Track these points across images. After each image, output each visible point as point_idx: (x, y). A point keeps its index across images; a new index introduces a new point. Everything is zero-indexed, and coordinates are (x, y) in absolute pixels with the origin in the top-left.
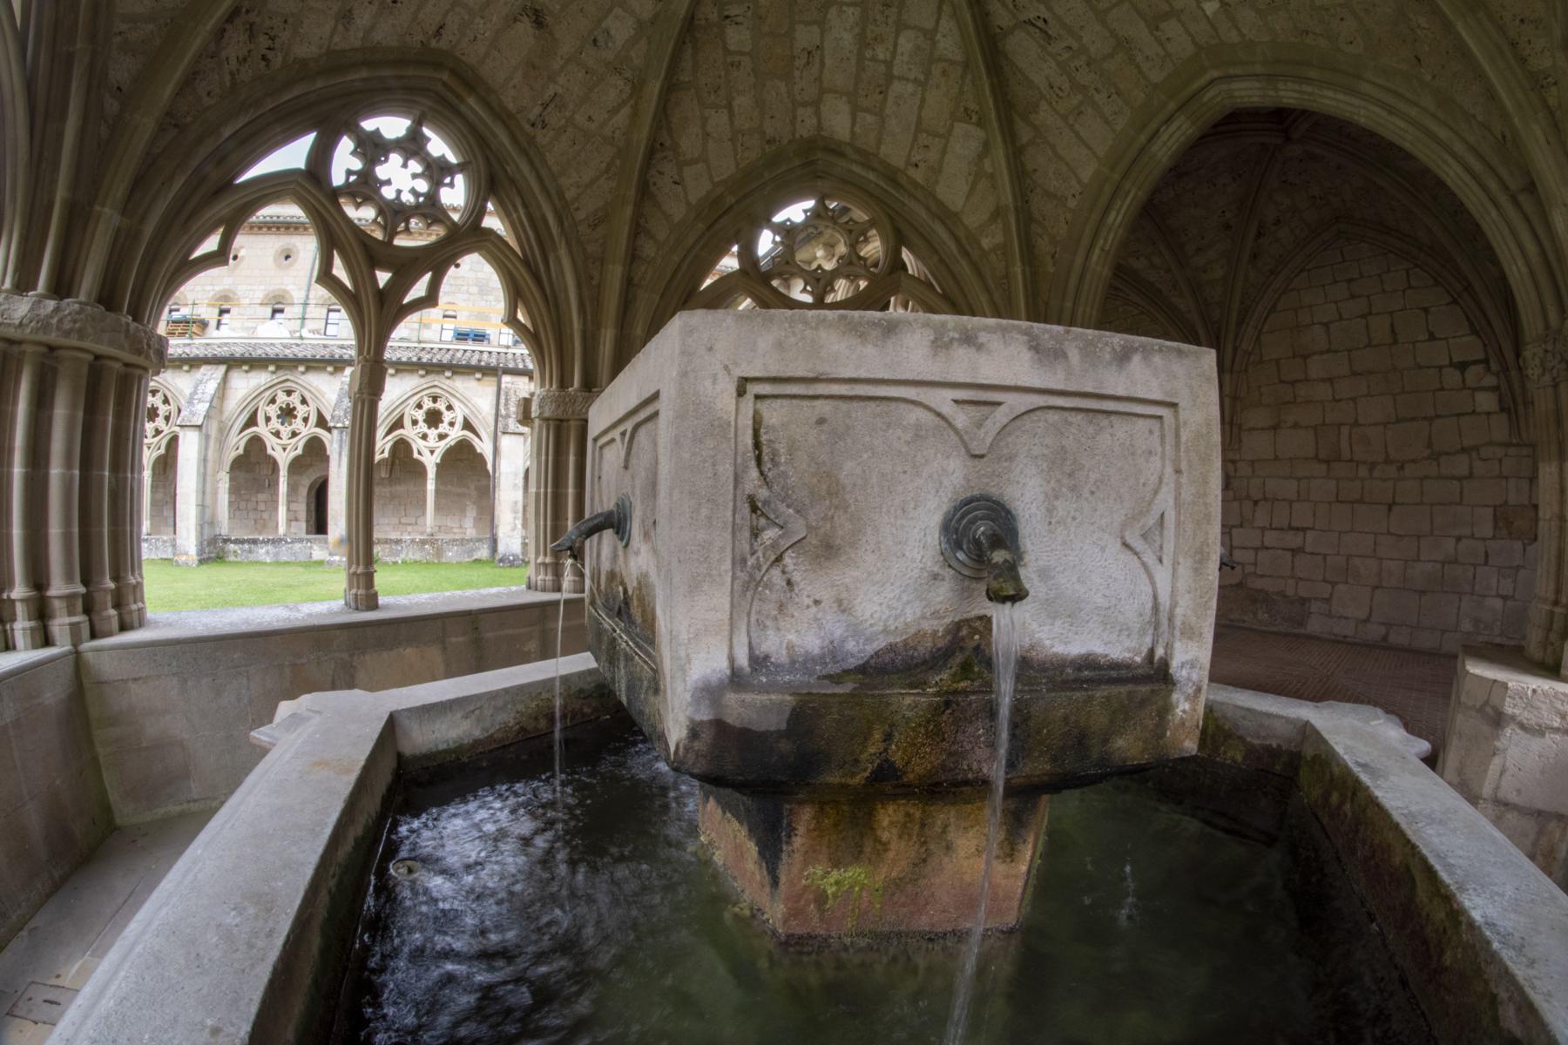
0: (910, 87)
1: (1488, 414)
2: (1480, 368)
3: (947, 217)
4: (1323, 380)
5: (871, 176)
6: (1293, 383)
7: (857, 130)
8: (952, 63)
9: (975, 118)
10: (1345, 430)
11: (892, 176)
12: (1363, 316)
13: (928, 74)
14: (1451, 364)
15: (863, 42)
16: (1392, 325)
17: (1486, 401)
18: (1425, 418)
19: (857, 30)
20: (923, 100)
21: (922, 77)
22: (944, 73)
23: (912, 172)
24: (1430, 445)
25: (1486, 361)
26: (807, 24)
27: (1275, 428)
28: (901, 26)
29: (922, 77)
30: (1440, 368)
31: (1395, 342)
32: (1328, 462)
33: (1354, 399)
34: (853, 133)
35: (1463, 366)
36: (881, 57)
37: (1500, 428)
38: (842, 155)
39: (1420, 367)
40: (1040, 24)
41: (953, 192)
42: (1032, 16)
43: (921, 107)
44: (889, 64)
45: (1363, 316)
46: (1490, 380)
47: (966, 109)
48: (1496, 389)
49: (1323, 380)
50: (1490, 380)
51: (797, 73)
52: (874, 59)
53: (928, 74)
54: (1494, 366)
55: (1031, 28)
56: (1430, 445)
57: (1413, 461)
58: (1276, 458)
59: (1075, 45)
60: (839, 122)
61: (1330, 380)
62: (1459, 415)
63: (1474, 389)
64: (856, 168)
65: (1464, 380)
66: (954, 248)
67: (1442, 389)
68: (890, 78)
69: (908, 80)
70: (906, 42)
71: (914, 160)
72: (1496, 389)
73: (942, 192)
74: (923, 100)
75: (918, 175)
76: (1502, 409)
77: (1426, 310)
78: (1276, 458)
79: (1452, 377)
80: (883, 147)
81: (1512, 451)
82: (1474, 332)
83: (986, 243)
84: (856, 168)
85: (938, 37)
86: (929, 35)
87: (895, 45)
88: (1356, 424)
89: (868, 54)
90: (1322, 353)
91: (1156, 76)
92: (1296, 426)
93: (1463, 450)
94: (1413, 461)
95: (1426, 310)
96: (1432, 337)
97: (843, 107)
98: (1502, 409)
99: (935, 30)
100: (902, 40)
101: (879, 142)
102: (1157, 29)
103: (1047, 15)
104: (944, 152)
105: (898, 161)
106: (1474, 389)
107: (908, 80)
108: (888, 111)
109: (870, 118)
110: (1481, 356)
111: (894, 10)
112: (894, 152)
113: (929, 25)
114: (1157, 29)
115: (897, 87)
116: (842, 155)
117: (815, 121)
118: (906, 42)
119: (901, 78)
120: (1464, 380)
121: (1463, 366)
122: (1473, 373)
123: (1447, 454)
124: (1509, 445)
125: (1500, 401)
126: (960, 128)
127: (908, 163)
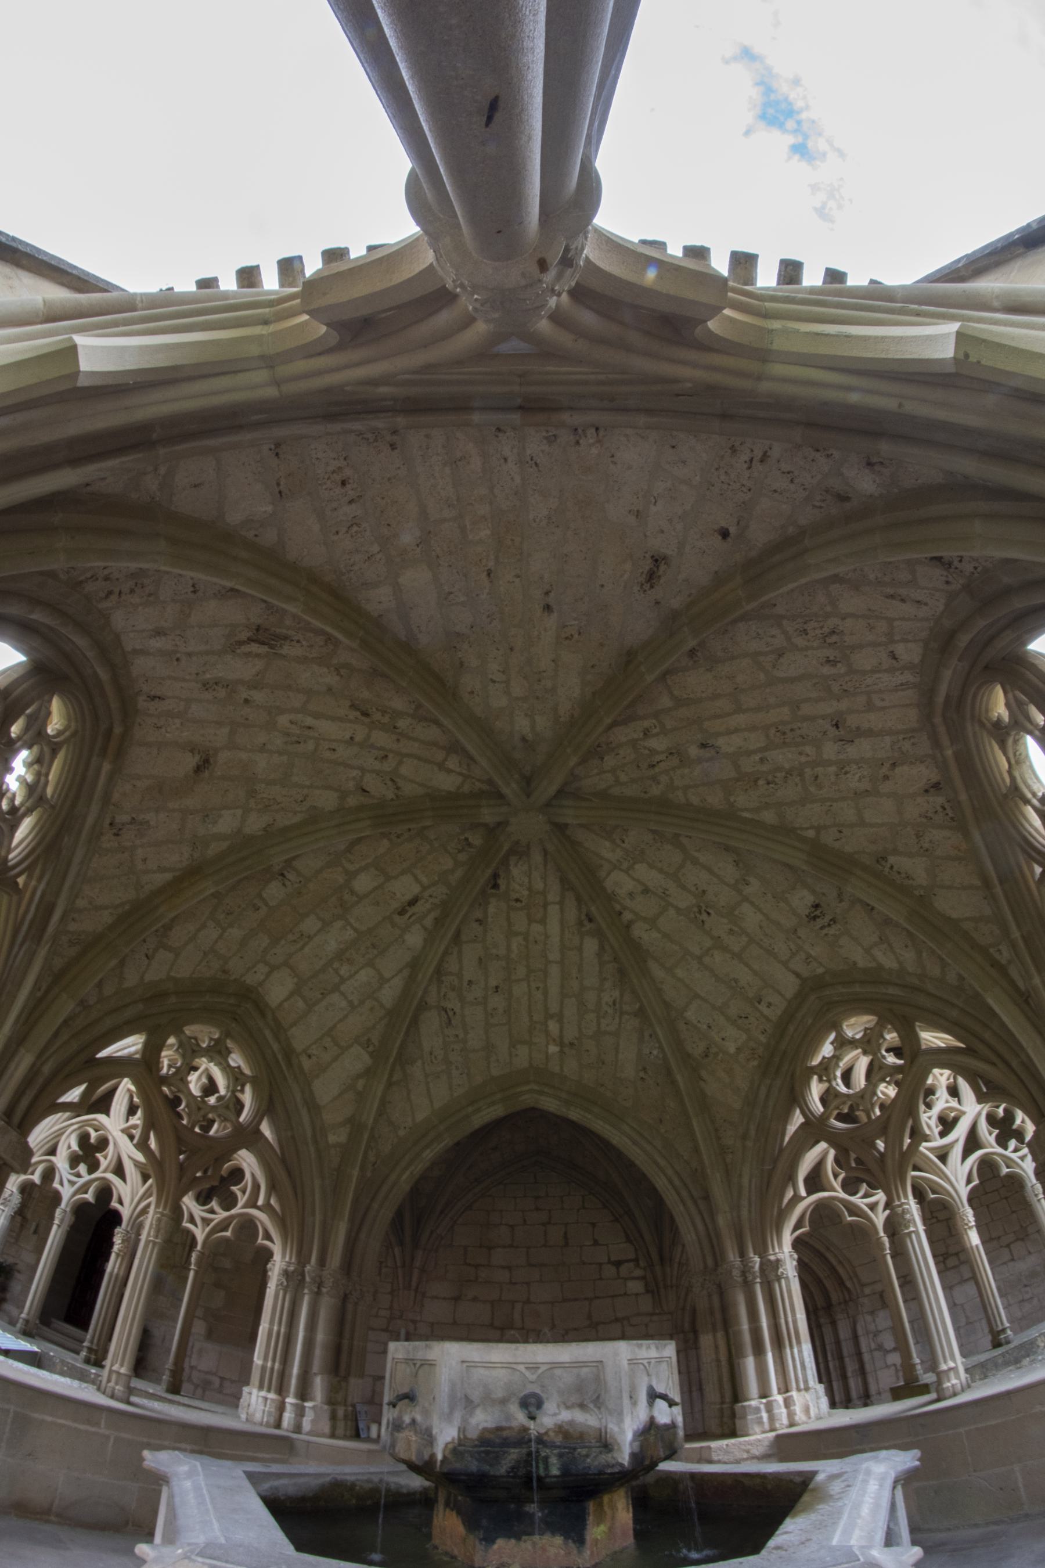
0: (344, 1004)
1: (637, 1295)
2: (631, 1265)
3: (313, 1107)
4: (503, 1267)
5: (276, 1047)
6: (477, 1266)
7: (286, 1005)
8: (382, 1006)
9: (371, 1049)
10: (518, 1306)
11: (289, 1053)
12: (543, 1224)
13: (362, 1002)
14: (609, 1262)
15: (340, 956)
16: (566, 1233)
17: (635, 1286)
18: (586, 1299)
19: (342, 946)
20: (346, 1017)
21: (356, 1003)
22: (372, 1009)
23: (304, 1059)
24: (589, 1317)
25: (636, 1260)
26: (416, 879)
27: (457, 1299)
28: (370, 964)
29: (356, 1003)
30: (600, 1264)
31: (567, 1245)
32: (502, 1329)
33: (528, 1284)
34: (281, 1004)
35: (618, 1264)
36: (342, 972)
37: (646, 1304)
38: (263, 1014)
39: (584, 1263)
40: (451, 1014)
41: (325, 1089)
42: (449, 1006)
43: (341, 1021)
44: (343, 980)
45: (543, 1224)
46: (638, 1273)
47: (369, 1040)
48: (643, 1278)
49: (503, 1267)
50: (638, 1273)
51: (283, 942)
52: (336, 971)
53: (362, 1002)
54: (642, 1263)
55: (443, 1013)
56: (589, 1317)
57: (575, 1329)
58: (455, 1323)
59: (461, 1036)
60: (277, 991)
61: (509, 1268)
62: (612, 1296)
63: (626, 1279)
64: (267, 1033)
65: (618, 1272)
66: (309, 1133)
67: (601, 1279)
68: (336, 988)
69: (346, 998)
70: (365, 975)
71: (310, 1052)
72: (643, 1278)
73: (317, 1085)
74: (346, 1017)
75: (306, 1064)
76: (647, 1291)
77: (594, 1225)
78: (455, 1323)
79: (609, 1271)
80: (294, 1029)
81: (655, 1318)
82: (629, 1240)
83: (332, 1139)
84: (267, 1033)
85: (387, 986)
86: (383, 981)
87: (356, 973)
88: (528, 1301)
89: (336, 965)
90: (505, 1247)
91: (495, 1072)
92: (475, 1299)
93: (617, 1320)
94: (575, 1329)
95: (594, 1225)
96: (596, 1243)
97: (290, 984)
98: (647, 1291)
99: (388, 980)
100: (363, 972)
101: (294, 1024)
102: (514, 1047)
103: (458, 1010)
104: (336, 1059)
105: (298, 1045)
106: (626, 1279)
107: (346, 998)
108: (316, 1008)
109: (301, 1004)
110: (632, 1256)
111: (375, 952)
112: (300, 1038)
113: (387, 975)
114: (514, 1047)
115: (335, 997)
116: (263, 1014)
117: (262, 978)
118: (365, 975)
119: (342, 994)
120: (618, 1272)
121: (618, 1264)
122: (624, 1269)
123: (604, 1323)
124: (652, 1314)
125: (646, 1285)
126: (356, 1050)
127: (304, 1051)
